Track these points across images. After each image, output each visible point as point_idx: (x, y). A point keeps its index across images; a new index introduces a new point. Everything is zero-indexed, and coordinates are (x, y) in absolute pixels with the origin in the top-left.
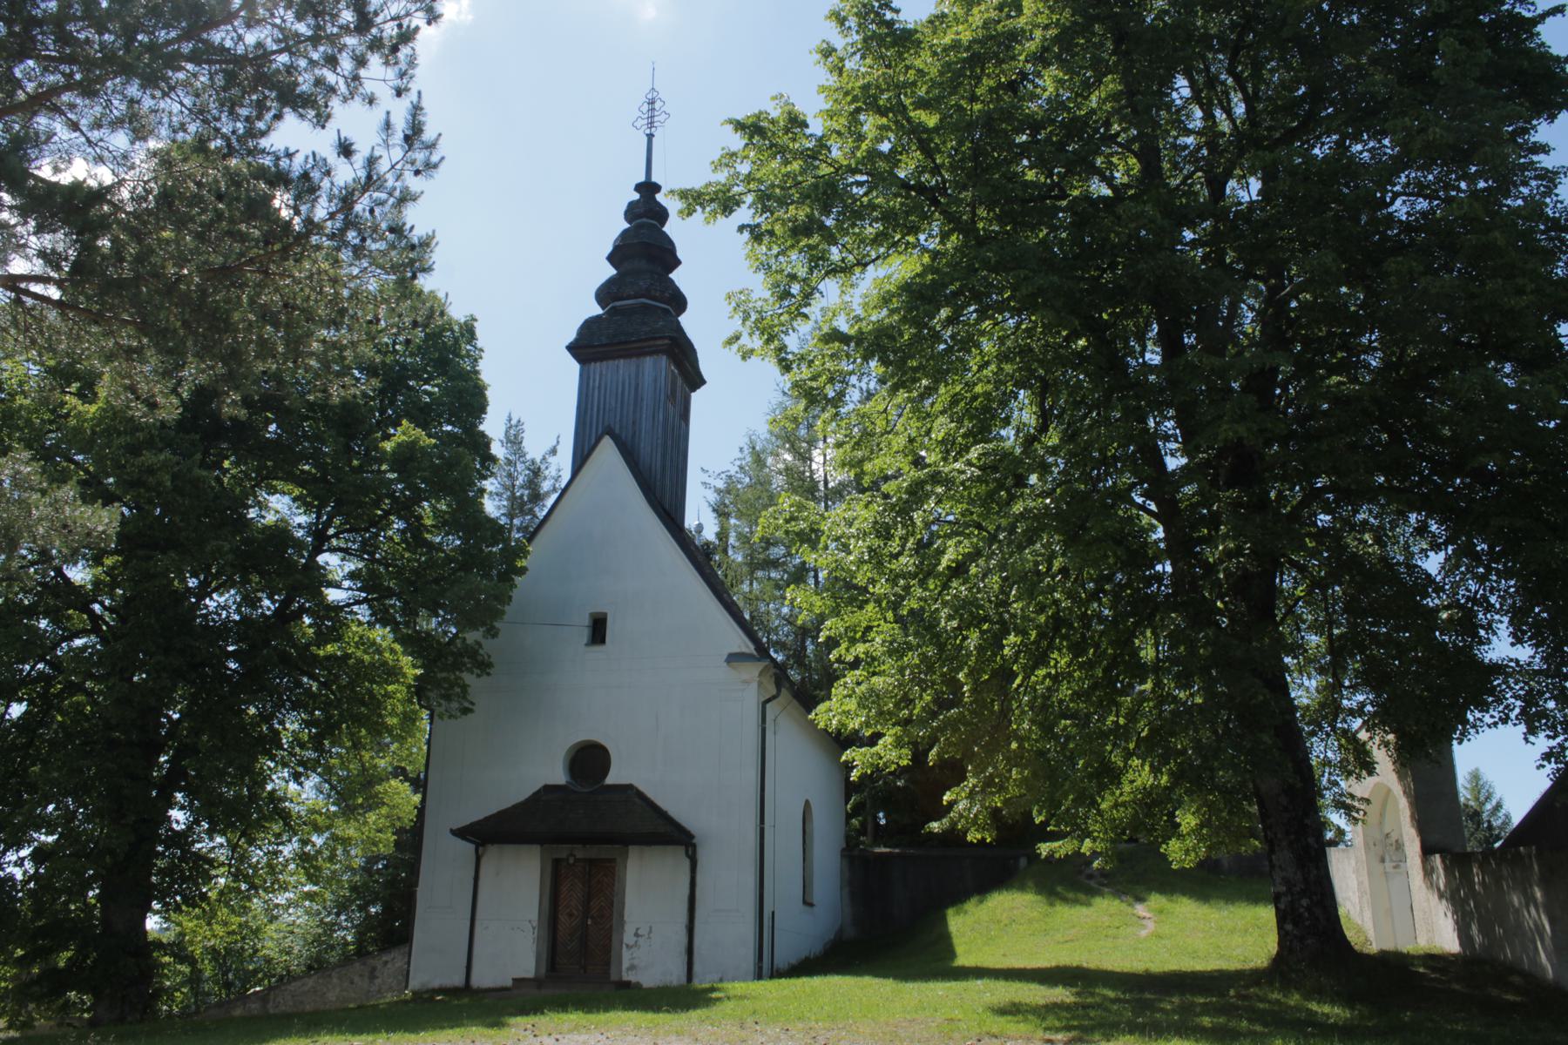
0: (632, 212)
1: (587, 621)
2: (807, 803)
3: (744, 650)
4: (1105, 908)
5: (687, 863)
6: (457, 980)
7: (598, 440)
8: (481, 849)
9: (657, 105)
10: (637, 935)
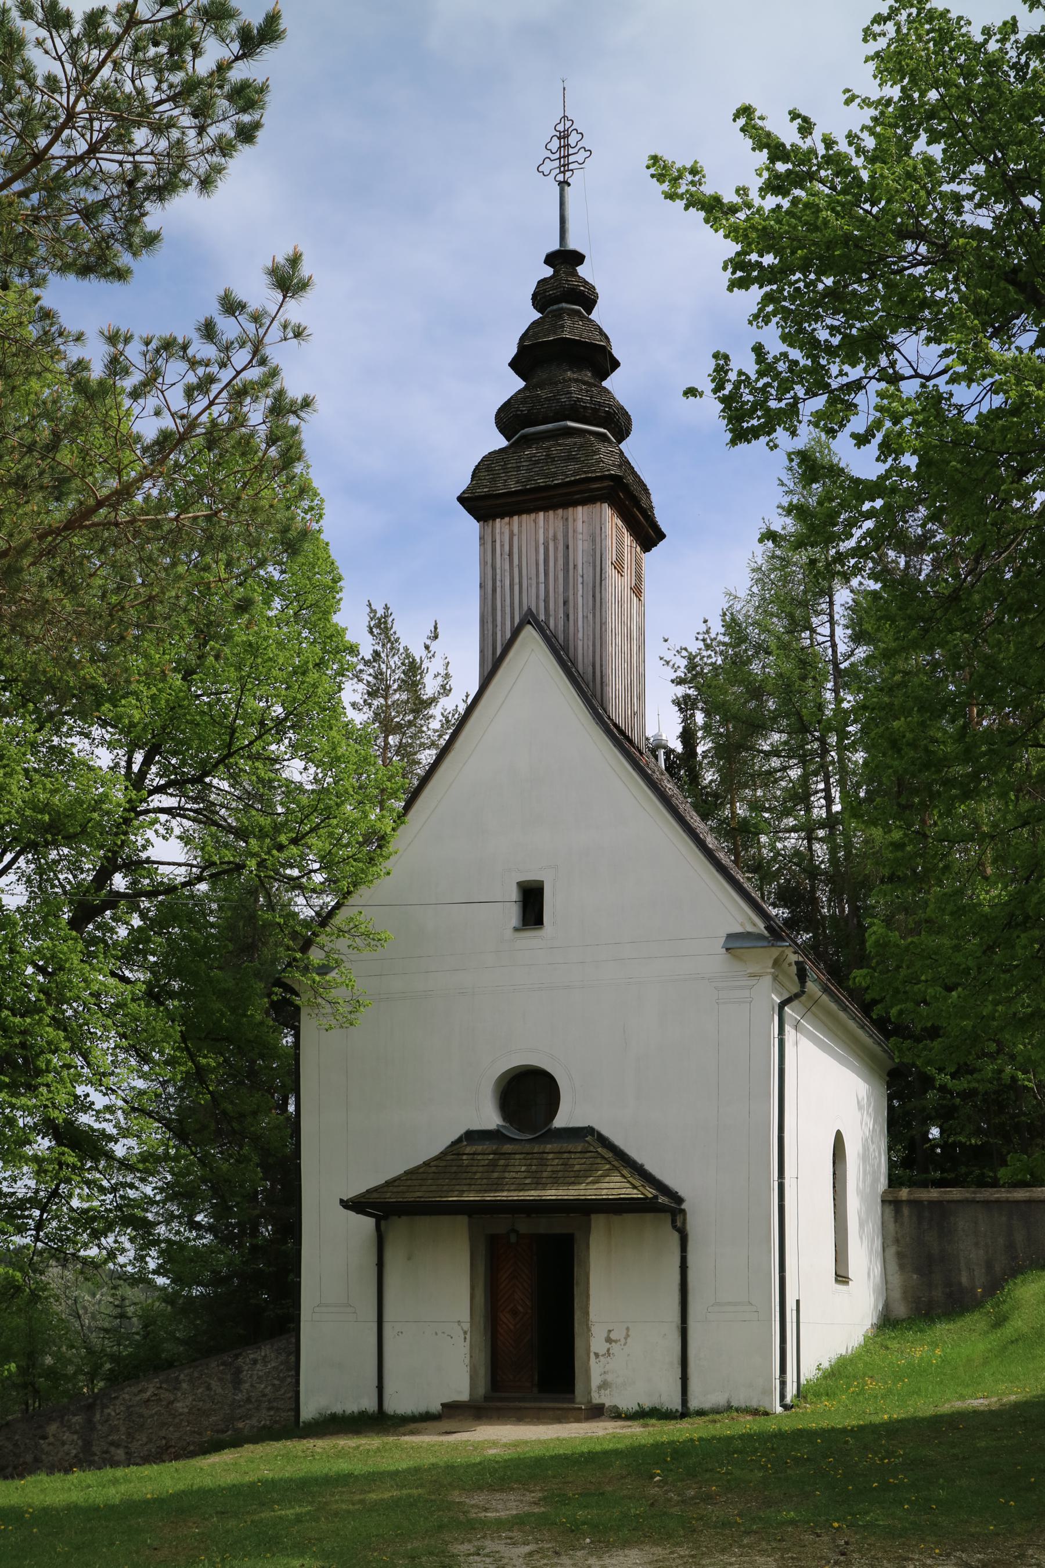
0: (542, 297)
1: (514, 894)
2: (839, 1139)
3: (750, 928)
4: (77, 1476)
5: (676, 1235)
6: (368, 1403)
7: (516, 633)
8: (383, 1223)
9: (573, 139)
10: (609, 1340)
